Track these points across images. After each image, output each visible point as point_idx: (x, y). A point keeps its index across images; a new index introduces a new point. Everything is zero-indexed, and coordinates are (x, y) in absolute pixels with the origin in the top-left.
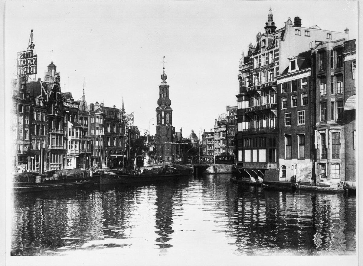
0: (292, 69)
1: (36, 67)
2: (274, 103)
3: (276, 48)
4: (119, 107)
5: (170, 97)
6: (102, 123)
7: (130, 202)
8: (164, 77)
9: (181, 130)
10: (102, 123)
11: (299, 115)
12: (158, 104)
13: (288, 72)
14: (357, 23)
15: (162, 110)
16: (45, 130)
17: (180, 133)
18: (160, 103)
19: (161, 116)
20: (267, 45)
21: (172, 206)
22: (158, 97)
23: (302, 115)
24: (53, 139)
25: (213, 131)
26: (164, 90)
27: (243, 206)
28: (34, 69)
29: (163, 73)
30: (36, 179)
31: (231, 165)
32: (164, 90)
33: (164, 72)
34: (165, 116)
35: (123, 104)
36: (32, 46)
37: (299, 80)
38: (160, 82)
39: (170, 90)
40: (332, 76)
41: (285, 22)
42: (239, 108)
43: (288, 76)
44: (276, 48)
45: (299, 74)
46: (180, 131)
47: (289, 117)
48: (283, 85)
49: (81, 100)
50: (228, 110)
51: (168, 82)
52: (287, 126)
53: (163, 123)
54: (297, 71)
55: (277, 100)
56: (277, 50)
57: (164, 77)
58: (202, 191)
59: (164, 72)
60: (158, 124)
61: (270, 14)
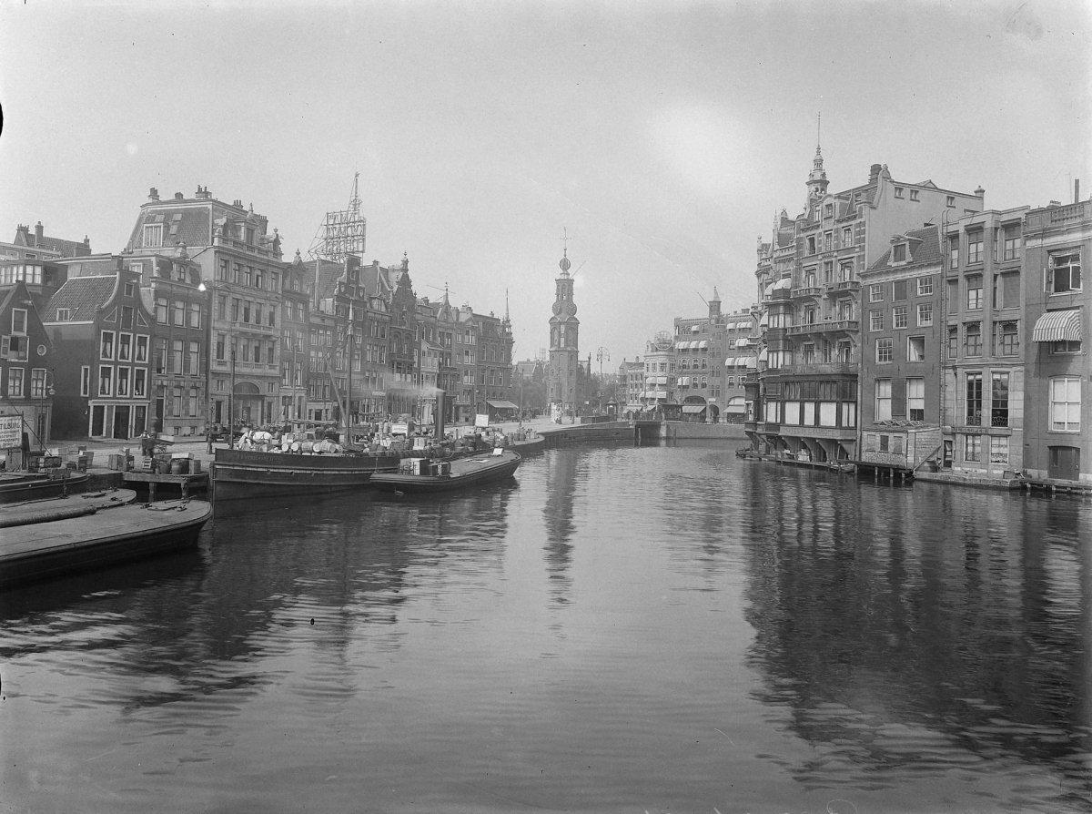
1: (364, 239)
3: (858, 221)
4: (500, 315)
5: (575, 300)
8: (565, 265)
15: (560, 323)
16: (74, 320)
18: (557, 309)
20: (838, 215)
21: (814, 549)
22: (554, 299)
25: (642, 360)
26: (565, 287)
28: (361, 245)
32: (565, 287)
36: (356, 203)
38: (558, 273)
41: (154, 193)
42: (771, 326)
43: (888, 273)
44: (858, 221)
49: (442, 301)
50: (677, 326)
52: (883, 363)
53: (562, 345)
54: (909, 263)
56: (863, 224)
60: (552, 346)
61: (818, 157)
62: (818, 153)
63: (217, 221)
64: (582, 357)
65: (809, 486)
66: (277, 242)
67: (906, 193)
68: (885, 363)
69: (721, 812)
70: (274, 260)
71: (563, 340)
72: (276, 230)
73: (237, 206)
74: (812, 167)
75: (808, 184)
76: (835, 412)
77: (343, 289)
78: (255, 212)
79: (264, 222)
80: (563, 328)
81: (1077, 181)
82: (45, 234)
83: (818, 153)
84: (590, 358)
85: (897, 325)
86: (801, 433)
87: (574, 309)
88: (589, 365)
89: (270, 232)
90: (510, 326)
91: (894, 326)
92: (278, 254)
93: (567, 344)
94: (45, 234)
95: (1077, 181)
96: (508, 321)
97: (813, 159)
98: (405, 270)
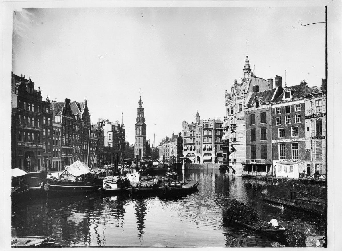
0: (286, 98)
2: (219, 134)
8: (140, 103)
11: (277, 110)
12: (137, 121)
13: (283, 99)
14: (122, 246)
18: (138, 120)
19: (139, 129)
23: (279, 110)
26: (141, 111)
27: (254, 236)
29: (139, 100)
32: (141, 111)
33: (140, 99)
35: (123, 121)
37: (293, 106)
38: (138, 106)
39: (144, 111)
40: (101, 171)
45: (292, 101)
47: (296, 130)
51: (143, 106)
57: (140, 103)
59: (140, 99)
61: (247, 60)
62: (247, 58)
63: (17, 84)
64: (147, 139)
68: (282, 137)
71: (140, 132)
73: (136, 125)
74: (245, 63)
75: (244, 70)
78: (230, 163)
80: (140, 127)
81: (326, 7)
83: (247, 58)
84: (150, 140)
85: (297, 122)
87: (144, 120)
88: (150, 142)
90: (124, 127)
91: (295, 123)
93: (142, 134)
95: (326, 7)
96: (123, 125)
97: (245, 60)
98: (86, 104)
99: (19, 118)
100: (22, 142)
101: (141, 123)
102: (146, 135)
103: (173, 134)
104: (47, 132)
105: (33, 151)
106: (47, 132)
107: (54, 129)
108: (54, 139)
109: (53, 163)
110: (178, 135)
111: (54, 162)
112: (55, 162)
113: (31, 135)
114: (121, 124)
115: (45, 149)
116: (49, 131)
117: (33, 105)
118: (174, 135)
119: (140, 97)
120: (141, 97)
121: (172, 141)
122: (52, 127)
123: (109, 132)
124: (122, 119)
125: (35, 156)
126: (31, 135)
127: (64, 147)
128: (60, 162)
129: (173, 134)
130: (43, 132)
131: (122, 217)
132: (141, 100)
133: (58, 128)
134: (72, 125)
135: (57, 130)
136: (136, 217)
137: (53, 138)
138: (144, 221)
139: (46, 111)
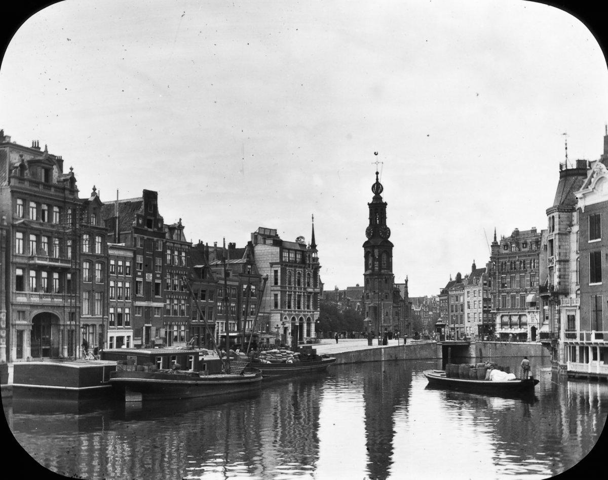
5: (389, 223)
6: (137, 255)
7: (544, 372)
8: (377, 188)
9: (407, 281)
10: (137, 255)
17: (405, 286)
22: (367, 223)
24: (81, 256)
26: (378, 209)
29: (375, 181)
30: (259, 269)
31: (281, 340)
32: (378, 209)
33: (377, 179)
34: (380, 256)
38: (370, 196)
46: (405, 283)
48: (68, 185)
51: (385, 196)
55: (581, 380)
57: (377, 188)
58: (472, 417)
59: (377, 179)
60: (366, 269)
65: (104, 325)
66: (72, 180)
67: (376, 333)
69: (607, 330)
70: (71, 197)
71: (377, 263)
72: (71, 169)
73: (365, 245)
76: (347, 351)
77: (140, 221)
78: (50, 152)
79: (60, 162)
82: (209, 245)
86: (18, 255)
87: (387, 232)
89: (66, 171)
92: (74, 191)
94: (218, 246)
99: (83, 239)
100: (27, 292)
101: (379, 241)
102: (392, 271)
103: (474, 266)
104: (92, 270)
105: (56, 312)
106: (92, 270)
107: (112, 262)
108: (112, 284)
109: (109, 339)
110: (485, 269)
111: (112, 338)
112: (115, 339)
113: (50, 278)
114: (308, 241)
115: (170, 310)
116: (98, 266)
117: (56, 209)
118: (477, 268)
119: (377, 173)
120: (379, 175)
121: (470, 283)
122: (108, 258)
123: (272, 264)
124: (494, 236)
125: (60, 325)
126: (50, 278)
127: (138, 303)
128: (129, 337)
129: (474, 266)
130: (80, 270)
131: (260, 462)
132: (379, 181)
133: (124, 259)
134: (164, 251)
135: (120, 263)
136: (369, 461)
137: (108, 283)
138: (393, 451)
139: (88, 222)
